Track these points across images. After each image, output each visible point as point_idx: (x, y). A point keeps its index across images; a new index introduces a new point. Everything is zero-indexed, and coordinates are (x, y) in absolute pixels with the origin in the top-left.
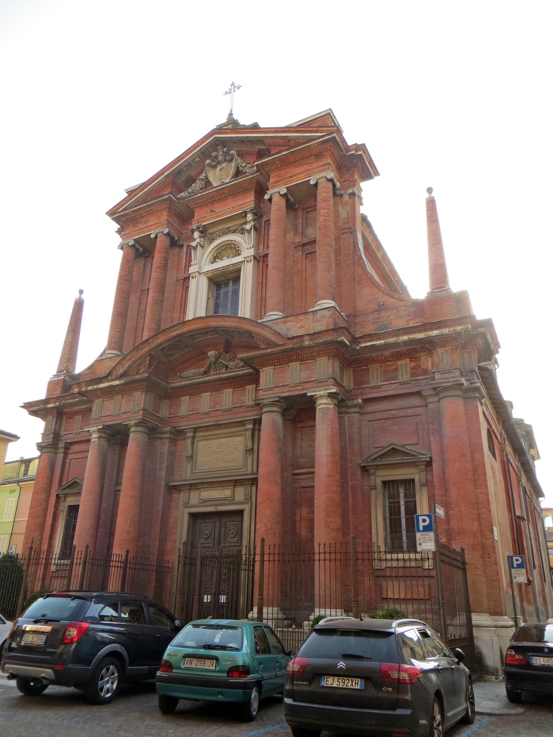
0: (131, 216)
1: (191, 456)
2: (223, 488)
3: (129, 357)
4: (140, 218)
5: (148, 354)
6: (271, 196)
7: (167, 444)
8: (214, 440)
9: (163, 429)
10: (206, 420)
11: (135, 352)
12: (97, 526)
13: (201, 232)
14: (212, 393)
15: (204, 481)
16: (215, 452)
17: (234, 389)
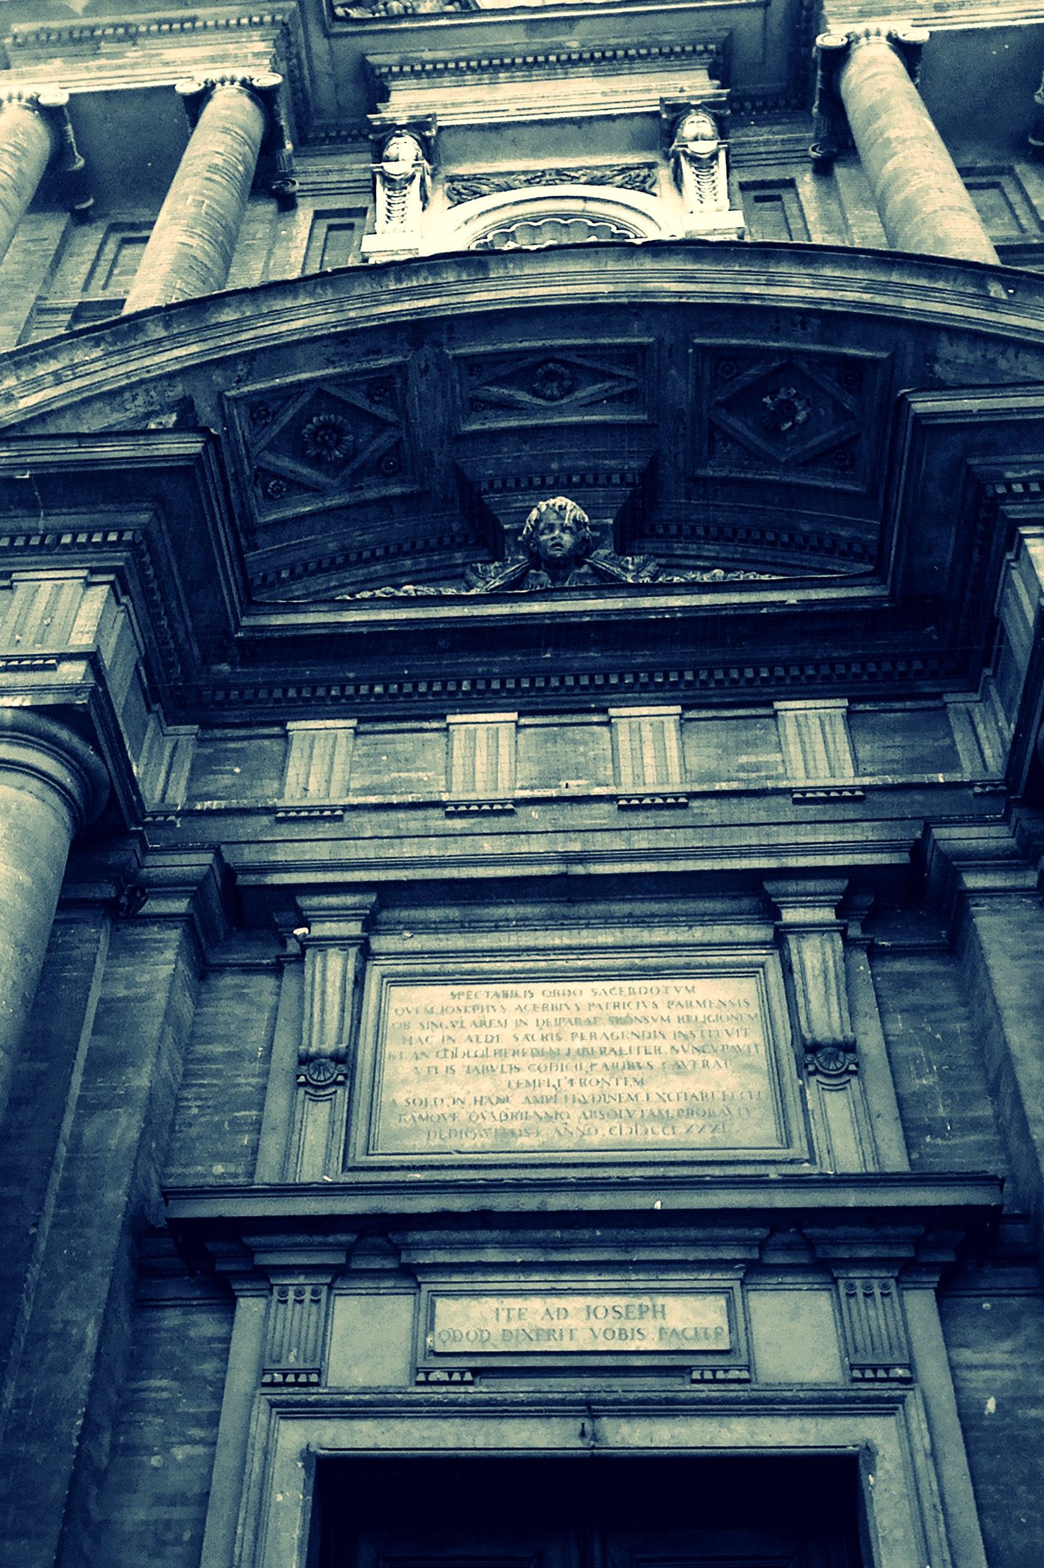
0: (75, 22)
1: (344, 1059)
2: (638, 1279)
3: (54, 366)
4: (120, 40)
5: (178, 390)
6: (849, 44)
7: (170, 955)
8: (521, 988)
9: (150, 860)
10: (488, 846)
11: (97, 353)
12: (776, 589)
13: (424, 143)
14: (523, 721)
15: (503, 1203)
16: (539, 1053)
17: (686, 708)
